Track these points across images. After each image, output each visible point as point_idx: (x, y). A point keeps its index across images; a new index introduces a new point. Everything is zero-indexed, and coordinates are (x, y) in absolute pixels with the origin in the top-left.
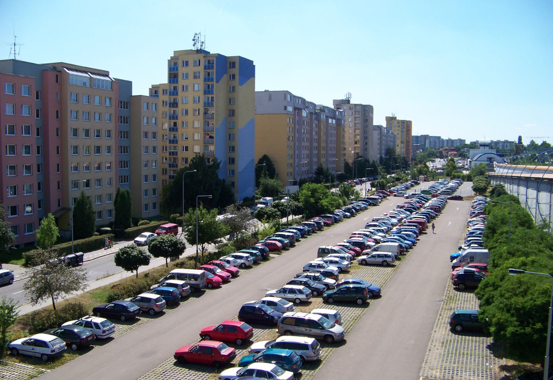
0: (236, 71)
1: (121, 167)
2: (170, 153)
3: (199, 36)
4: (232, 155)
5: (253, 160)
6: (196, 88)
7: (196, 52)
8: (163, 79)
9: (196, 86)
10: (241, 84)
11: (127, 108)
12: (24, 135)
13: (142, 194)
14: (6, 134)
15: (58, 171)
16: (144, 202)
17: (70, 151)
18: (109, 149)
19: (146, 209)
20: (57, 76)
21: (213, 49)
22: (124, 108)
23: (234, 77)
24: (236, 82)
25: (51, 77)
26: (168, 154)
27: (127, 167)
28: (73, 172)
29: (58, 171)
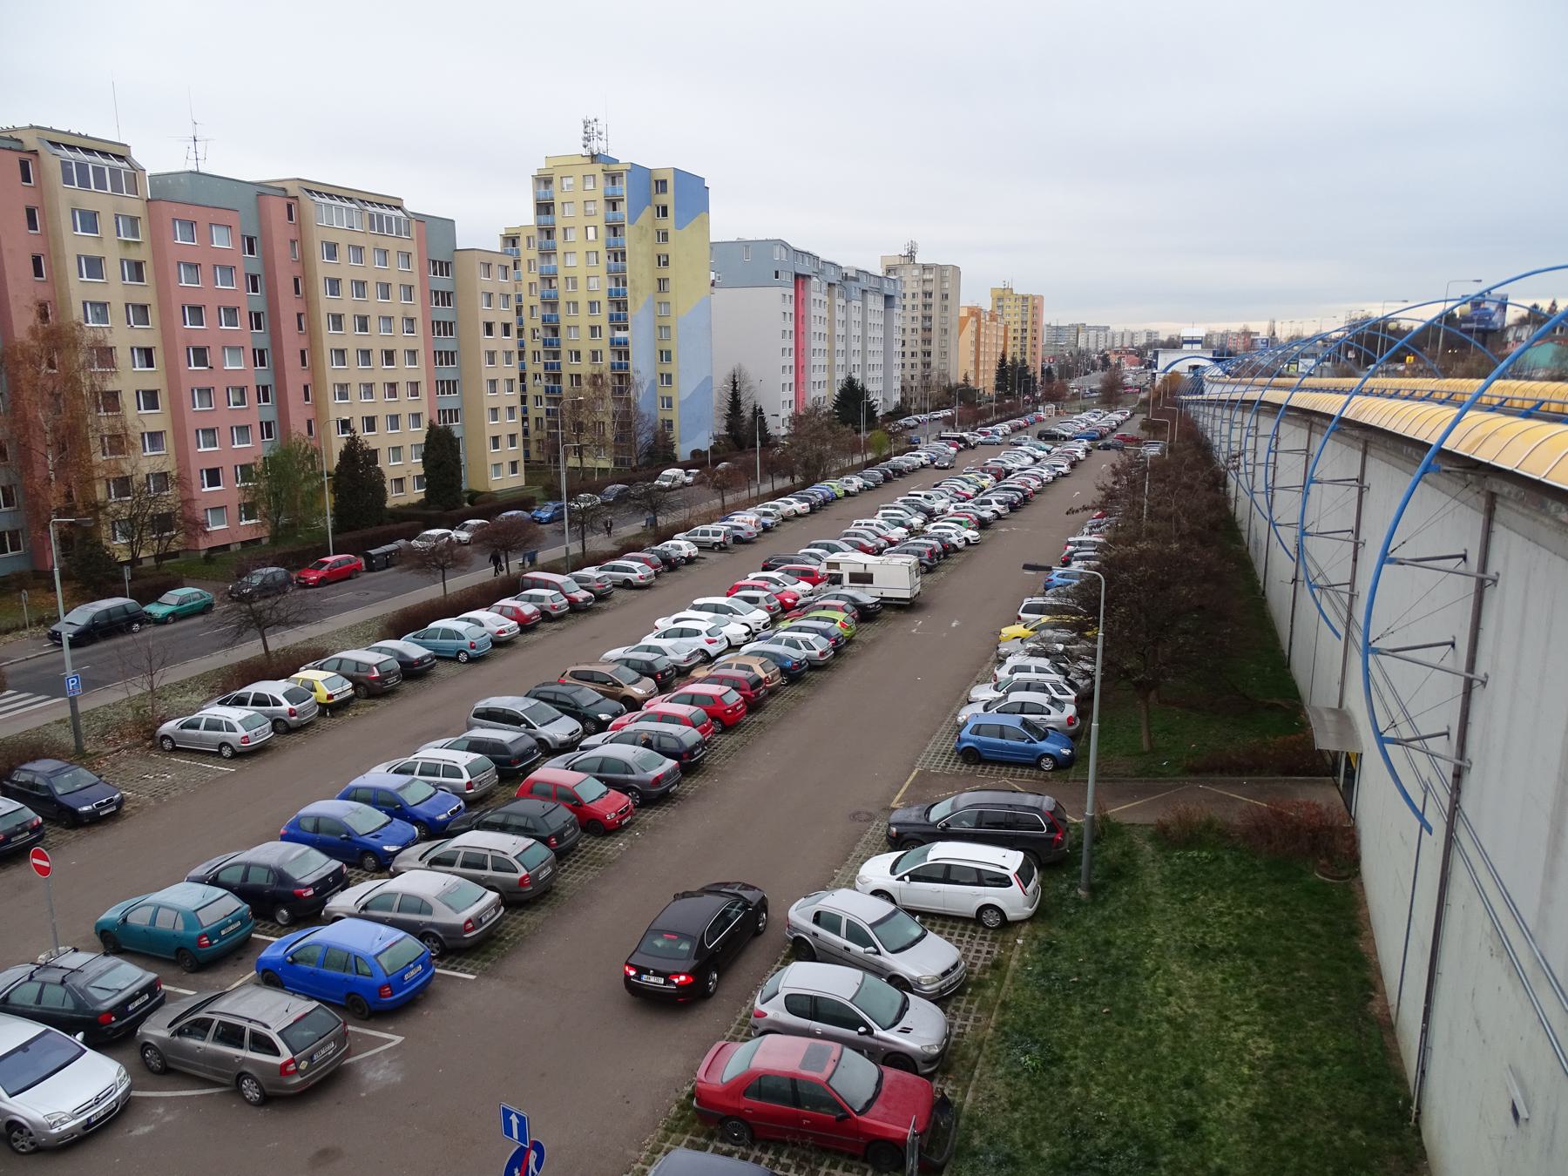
0: (668, 199)
1: (439, 334)
2: (546, 364)
3: (595, 126)
4: (667, 369)
5: (709, 379)
6: (591, 235)
7: (588, 160)
8: (524, 215)
9: (591, 231)
10: (680, 225)
11: (448, 275)
12: (224, 327)
13: (483, 359)
14: (190, 365)
15: (307, 399)
16: (489, 433)
17: (322, 288)
18: (415, 386)
19: (496, 446)
20: (289, 207)
21: (626, 150)
22: (447, 364)
23: (664, 211)
24: (669, 223)
25: (277, 208)
26: (542, 366)
27: (455, 392)
28: (337, 401)
29: (307, 399)
